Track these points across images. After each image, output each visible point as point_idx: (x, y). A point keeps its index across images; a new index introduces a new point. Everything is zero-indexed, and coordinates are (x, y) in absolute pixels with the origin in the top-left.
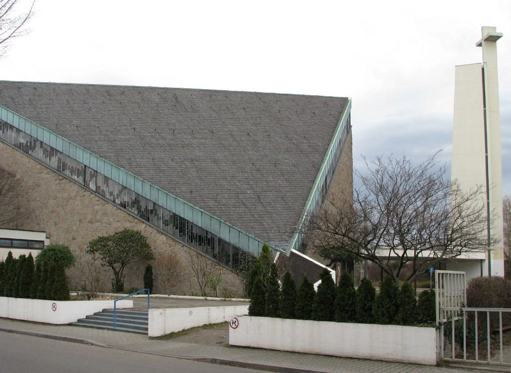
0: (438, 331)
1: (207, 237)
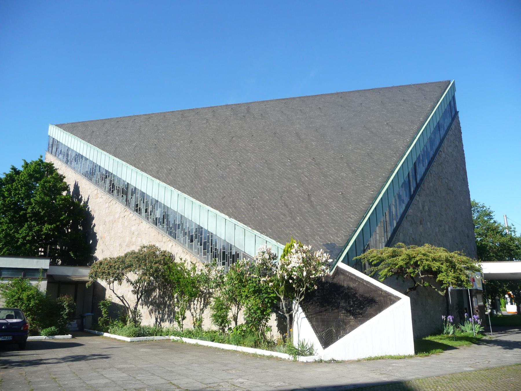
0: (125, 196)
1: (231, 252)
